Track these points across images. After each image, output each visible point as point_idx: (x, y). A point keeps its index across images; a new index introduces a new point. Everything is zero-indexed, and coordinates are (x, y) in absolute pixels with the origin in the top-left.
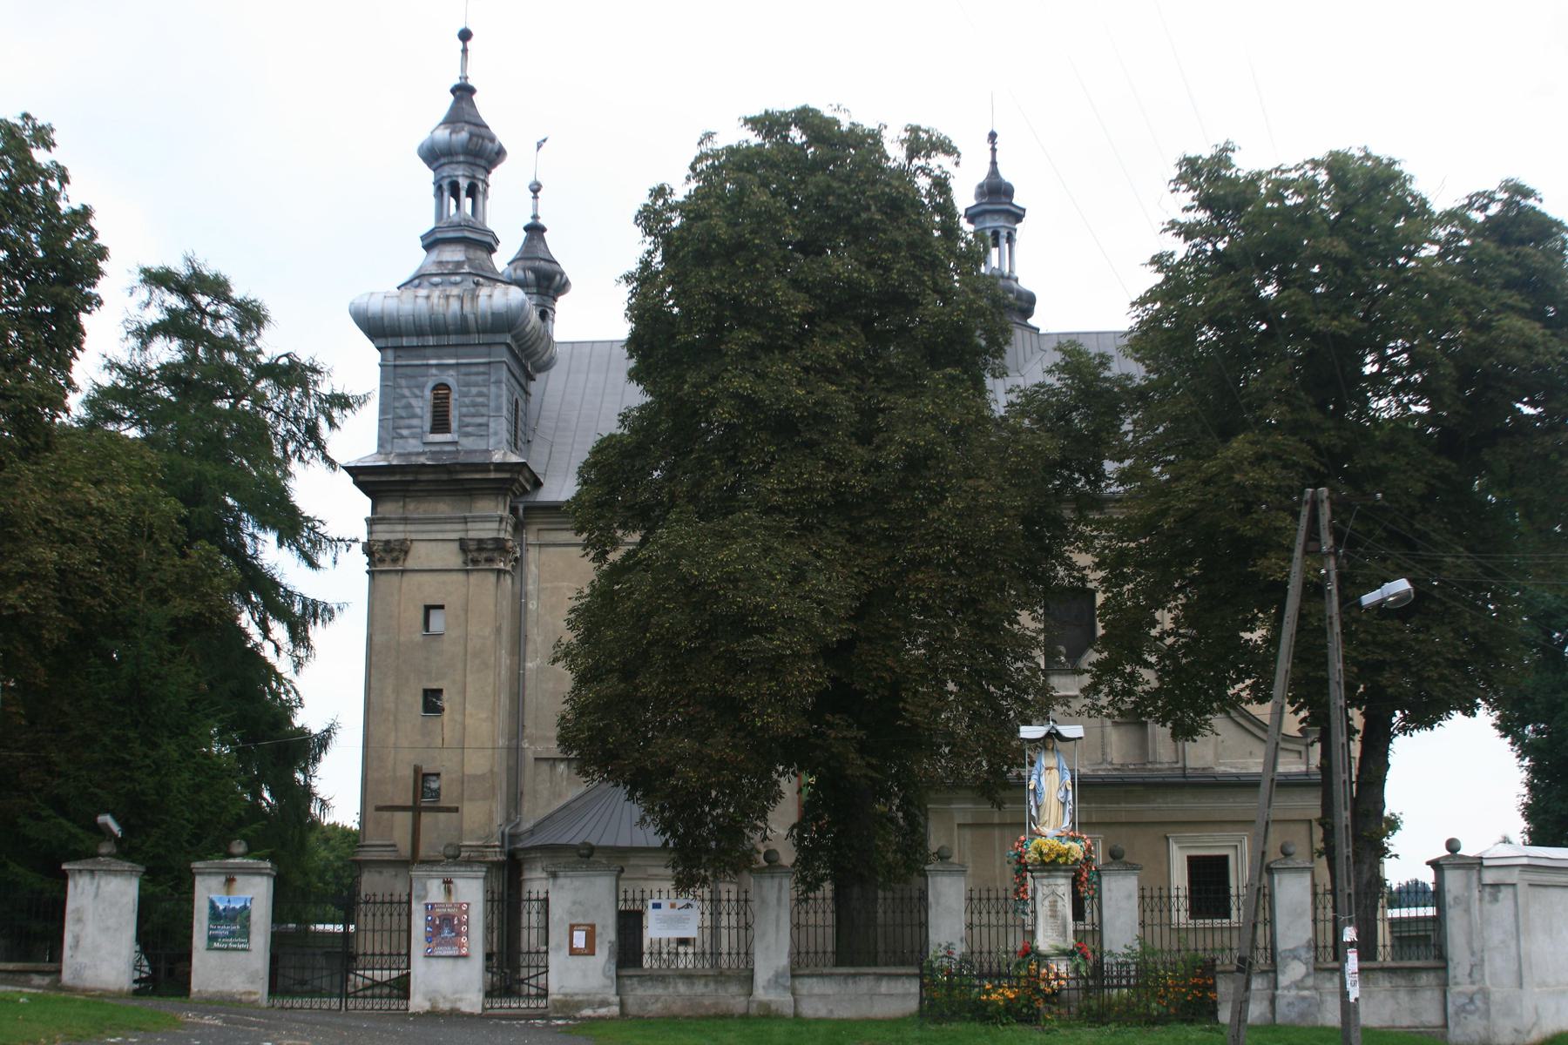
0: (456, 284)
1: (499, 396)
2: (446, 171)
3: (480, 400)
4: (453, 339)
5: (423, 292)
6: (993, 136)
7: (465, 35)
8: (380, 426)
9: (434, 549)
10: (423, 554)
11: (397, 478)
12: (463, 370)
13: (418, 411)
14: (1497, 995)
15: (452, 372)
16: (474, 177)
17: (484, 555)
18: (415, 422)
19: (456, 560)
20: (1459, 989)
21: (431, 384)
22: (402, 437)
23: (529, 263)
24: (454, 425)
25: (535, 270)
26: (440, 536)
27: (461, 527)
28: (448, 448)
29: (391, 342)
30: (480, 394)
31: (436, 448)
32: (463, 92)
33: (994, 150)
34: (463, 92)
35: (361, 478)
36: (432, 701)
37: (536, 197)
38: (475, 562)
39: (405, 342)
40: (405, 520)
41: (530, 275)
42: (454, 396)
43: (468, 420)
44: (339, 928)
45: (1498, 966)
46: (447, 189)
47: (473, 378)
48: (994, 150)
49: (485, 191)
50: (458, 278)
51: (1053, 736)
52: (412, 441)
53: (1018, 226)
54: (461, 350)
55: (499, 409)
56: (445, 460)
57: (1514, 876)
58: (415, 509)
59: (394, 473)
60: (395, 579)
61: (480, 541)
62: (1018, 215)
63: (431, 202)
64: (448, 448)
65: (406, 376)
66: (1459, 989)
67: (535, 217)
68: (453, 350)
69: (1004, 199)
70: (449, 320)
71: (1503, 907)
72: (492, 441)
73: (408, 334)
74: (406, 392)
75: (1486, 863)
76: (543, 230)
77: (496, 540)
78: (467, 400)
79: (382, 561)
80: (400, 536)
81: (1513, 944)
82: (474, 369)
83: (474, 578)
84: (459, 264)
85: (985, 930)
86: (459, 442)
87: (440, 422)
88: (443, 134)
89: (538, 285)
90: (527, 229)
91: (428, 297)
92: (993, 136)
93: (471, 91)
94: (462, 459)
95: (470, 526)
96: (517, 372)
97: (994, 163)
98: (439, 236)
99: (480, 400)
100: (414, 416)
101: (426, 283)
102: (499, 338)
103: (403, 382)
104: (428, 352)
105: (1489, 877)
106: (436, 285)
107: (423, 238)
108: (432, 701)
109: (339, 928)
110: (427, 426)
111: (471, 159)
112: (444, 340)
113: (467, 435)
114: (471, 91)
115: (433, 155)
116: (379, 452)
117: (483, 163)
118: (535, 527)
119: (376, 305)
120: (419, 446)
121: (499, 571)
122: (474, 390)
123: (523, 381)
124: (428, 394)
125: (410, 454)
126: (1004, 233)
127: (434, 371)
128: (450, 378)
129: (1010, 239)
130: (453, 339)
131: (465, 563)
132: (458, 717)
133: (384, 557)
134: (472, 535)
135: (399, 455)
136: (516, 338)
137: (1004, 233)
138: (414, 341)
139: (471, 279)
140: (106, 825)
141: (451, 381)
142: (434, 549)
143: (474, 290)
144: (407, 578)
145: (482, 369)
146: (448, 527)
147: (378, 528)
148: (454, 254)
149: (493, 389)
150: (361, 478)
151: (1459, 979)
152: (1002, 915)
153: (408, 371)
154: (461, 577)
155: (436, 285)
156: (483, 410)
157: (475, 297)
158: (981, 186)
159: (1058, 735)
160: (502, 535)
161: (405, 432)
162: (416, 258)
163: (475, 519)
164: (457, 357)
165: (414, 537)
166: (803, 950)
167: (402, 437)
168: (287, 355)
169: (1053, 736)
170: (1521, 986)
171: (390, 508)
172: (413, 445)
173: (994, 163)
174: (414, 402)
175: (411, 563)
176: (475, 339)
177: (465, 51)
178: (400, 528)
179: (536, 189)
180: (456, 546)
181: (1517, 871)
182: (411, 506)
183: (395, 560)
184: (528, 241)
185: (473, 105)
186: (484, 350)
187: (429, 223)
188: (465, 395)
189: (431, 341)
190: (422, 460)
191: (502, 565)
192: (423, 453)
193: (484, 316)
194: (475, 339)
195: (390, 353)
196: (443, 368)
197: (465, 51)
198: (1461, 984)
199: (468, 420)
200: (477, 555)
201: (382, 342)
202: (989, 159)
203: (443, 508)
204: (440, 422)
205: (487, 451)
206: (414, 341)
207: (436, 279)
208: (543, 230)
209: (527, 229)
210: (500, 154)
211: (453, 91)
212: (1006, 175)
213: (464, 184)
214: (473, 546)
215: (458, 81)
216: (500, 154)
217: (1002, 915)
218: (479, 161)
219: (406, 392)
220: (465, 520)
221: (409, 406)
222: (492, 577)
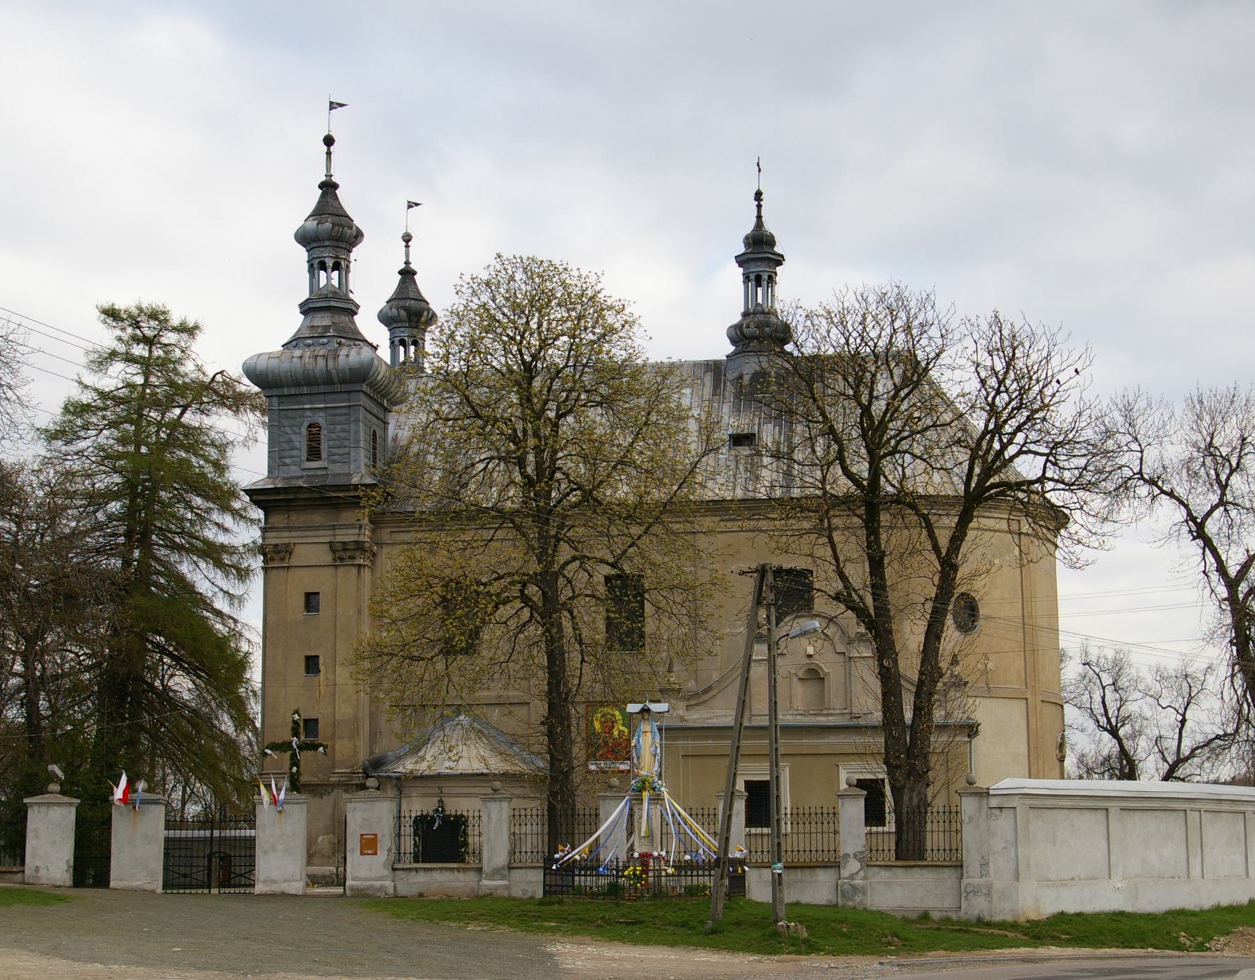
0: (324, 344)
1: (357, 432)
2: (317, 253)
3: (343, 435)
4: (322, 389)
5: (298, 353)
6: (758, 196)
7: (329, 141)
8: (269, 457)
9: (311, 550)
10: (303, 554)
11: (282, 497)
12: (331, 412)
13: (297, 444)
14: (998, 885)
15: (321, 414)
16: (337, 257)
17: (348, 554)
18: (295, 453)
19: (327, 558)
20: (970, 880)
21: (306, 424)
22: (286, 465)
23: (401, 303)
24: (324, 455)
25: (406, 309)
26: (315, 540)
27: (330, 532)
28: (320, 473)
29: (275, 392)
30: (343, 431)
31: (312, 473)
32: (328, 187)
33: (759, 206)
34: (328, 187)
35: (255, 498)
36: (312, 664)
37: (407, 246)
38: (341, 559)
39: (286, 391)
40: (289, 529)
41: (403, 313)
42: (323, 432)
43: (334, 451)
44: (208, 833)
45: (1000, 864)
46: (316, 266)
47: (337, 418)
48: (759, 206)
49: (348, 266)
50: (325, 340)
51: (645, 711)
52: (293, 468)
53: (779, 269)
54: (328, 397)
55: (358, 441)
56: (317, 482)
57: (1015, 802)
58: (297, 519)
59: (279, 494)
60: (282, 573)
61: (344, 543)
62: (779, 260)
63: (306, 276)
64: (320, 473)
65: (287, 418)
66: (970, 880)
67: (407, 263)
68: (322, 397)
69: (766, 249)
70: (318, 375)
71: (1003, 824)
72: (353, 466)
73: (288, 386)
74: (288, 430)
75: (991, 792)
76: (414, 273)
77: (356, 542)
78: (333, 436)
79: (273, 560)
80: (286, 541)
81: (1013, 850)
82: (338, 411)
83: (341, 571)
84: (326, 328)
85: (820, 836)
86: (328, 468)
87: (314, 453)
88: (312, 224)
89: (410, 320)
90: (401, 272)
91: (301, 357)
92: (758, 196)
93: (335, 186)
94: (329, 481)
95: (337, 532)
96: (375, 409)
97: (759, 217)
98: (311, 305)
99: (343, 435)
100: (294, 449)
101: (301, 345)
102: (357, 387)
103: (286, 422)
104: (304, 399)
105: (994, 802)
106: (309, 346)
107: (301, 306)
108: (312, 664)
109: (208, 833)
110: (304, 457)
111: (335, 244)
112: (315, 389)
113: (334, 462)
114: (335, 186)
115: (304, 238)
116: (269, 477)
117: (344, 245)
118: (388, 530)
119: (262, 365)
120: (300, 472)
121: (360, 566)
122: (339, 427)
123: (381, 416)
124: (304, 431)
125: (292, 478)
126: (765, 276)
127: (308, 413)
128: (320, 419)
129: (771, 280)
130: (322, 389)
131: (334, 560)
132: (331, 677)
133: (275, 556)
134: (338, 539)
135: (284, 478)
136: (371, 385)
137: (765, 276)
138: (293, 391)
139: (335, 340)
140: (53, 772)
141: (321, 421)
142: (311, 550)
143: (336, 350)
144: (292, 570)
145: (344, 411)
146: (321, 533)
147: (268, 534)
148: (323, 320)
149: (353, 426)
150: (255, 498)
151: (971, 874)
152: (807, 825)
153: (289, 414)
154: (332, 570)
155: (309, 346)
156: (346, 443)
157: (336, 357)
158: (747, 238)
159: (648, 710)
160: (362, 538)
161: (287, 461)
162: (293, 322)
163: (340, 527)
164: (325, 402)
165: (296, 541)
166: (874, 848)
167: (286, 465)
168: (221, 372)
169: (645, 711)
170: (1018, 880)
171: (277, 519)
172: (294, 471)
173: (759, 217)
174: (293, 437)
175: (294, 561)
176: (338, 388)
177: (329, 154)
178: (286, 534)
179: (407, 239)
180: (326, 547)
181: (1017, 798)
182: (294, 518)
183: (282, 559)
184: (402, 282)
185: (336, 198)
186: (345, 396)
187: (305, 295)
188: (331, 432)
189: (305, 390)
190: (301, 483)
191: (361, 561)
192: (302, 477)
193: (344, 370)
194: (338, 388)
195: (275, 400)
196: (316, 411)
197: (329, 154)
198: (972, 878)
199: (334, 451)
200: (344, 554)
201: (269, 393)
202: (756, 214)
203: (317, 518)
204: (314, 453)
205: (349, 474)
206: (293, 391)
207: (310, 341)
208: (414, 273)
209: (401, 272)
210: (359, 235)
211: (321, 186)
212: (770, 226)
213: (330, 263)
214: (339, 547)
215: (324, 179)
216: (359, 235)
217: (807, 825)
218: (341, 244)
219: (288, 430)
220: (334, 528)
221: (290, 441)
222: (354, 571)
